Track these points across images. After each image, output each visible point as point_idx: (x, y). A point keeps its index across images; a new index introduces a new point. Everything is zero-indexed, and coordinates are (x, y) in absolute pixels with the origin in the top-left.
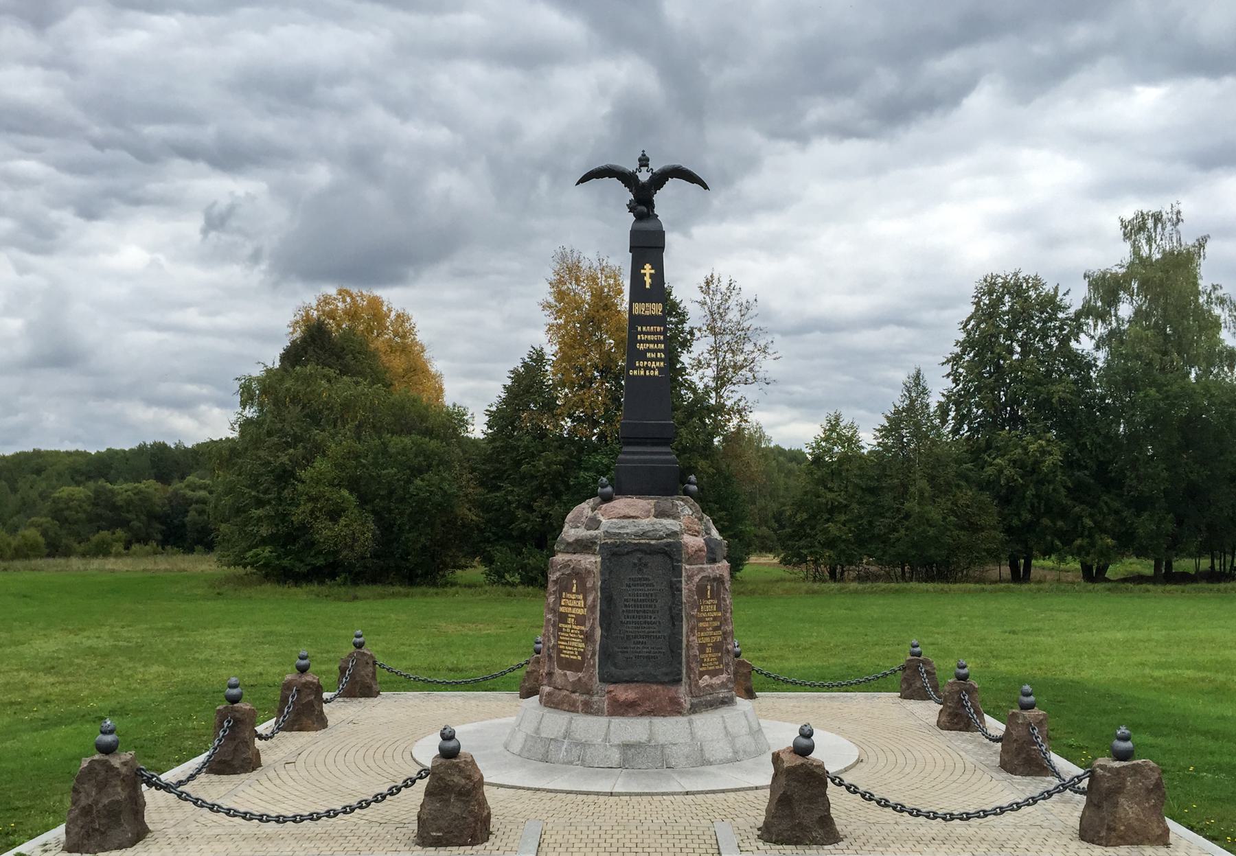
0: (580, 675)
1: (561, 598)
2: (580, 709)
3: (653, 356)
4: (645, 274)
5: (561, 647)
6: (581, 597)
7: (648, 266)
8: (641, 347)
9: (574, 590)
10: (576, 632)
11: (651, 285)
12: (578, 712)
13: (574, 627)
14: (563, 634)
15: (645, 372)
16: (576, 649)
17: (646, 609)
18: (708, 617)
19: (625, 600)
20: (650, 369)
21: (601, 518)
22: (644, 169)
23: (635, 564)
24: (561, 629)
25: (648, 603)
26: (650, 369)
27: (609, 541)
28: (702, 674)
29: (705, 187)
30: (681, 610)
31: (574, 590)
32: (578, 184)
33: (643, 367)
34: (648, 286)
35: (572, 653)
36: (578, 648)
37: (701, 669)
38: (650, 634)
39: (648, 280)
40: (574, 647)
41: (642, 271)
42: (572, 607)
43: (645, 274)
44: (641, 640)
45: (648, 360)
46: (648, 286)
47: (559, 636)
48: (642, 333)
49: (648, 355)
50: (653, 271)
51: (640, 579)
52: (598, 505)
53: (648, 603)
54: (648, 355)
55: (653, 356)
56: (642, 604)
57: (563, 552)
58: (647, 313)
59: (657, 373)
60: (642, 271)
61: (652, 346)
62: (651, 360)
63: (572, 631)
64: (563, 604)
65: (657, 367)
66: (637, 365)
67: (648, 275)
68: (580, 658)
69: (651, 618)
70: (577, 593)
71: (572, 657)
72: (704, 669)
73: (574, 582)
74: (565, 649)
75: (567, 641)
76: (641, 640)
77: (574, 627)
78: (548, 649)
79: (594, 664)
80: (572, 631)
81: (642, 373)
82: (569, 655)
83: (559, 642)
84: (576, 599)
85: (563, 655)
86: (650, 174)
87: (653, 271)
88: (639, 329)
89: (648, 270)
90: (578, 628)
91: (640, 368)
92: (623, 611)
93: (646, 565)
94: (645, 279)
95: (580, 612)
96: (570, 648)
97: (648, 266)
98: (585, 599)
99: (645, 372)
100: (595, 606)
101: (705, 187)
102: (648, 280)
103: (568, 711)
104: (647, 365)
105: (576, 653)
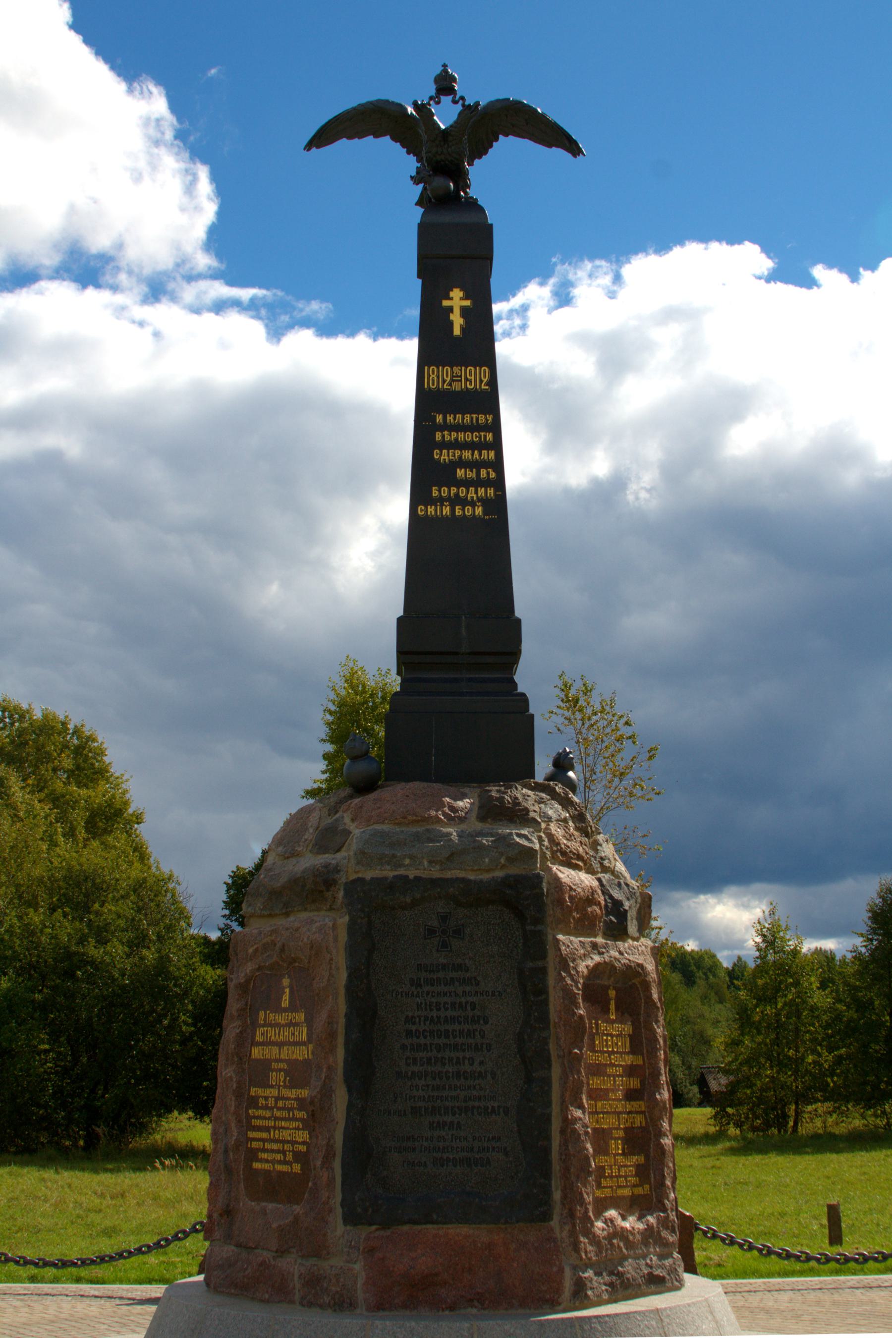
0: (297, 1209)
1: (255, 1025)
2: (297, 1297)
3: (471, 474)
4: (450, 309)
5: (255, 1145)
6: (301, 1017)
7: (456, 294)
8: (444, 456)
9: (285, 1003)
10: (288, 1104)
11: (462, 329)
12: (292, 1302)
13: (286, 1093)
14: (259, 1112)
15: (453, 511)
16: (287, 1147)
17: (460, 1040)
18: (612, 1065)
19: (408, 1020)
20: (464, 502)
21: (352, 827)
22: (446, 100)
23: (431, 932)
24: (253, 1102)
25: (466, 1027)
26: (464, 502)
27: (369, 875)
28: (601, 1206)
29: (573, 148)
30: (545, 1041)
31: (285, 1003)
32: (309, 146)
33: (449, 499)
34: (457, 331)
35: (279, 1157)
36: (293, 1143)
37: (598, 1193)
38: (470, 1104)
39: (457, 321)
40: (284, 1142)
41: (446, 303)
42: (280, 1045)
43: (450, 309)
44: (448, 1119)
45: (459, 483)
46: (457, 331)
47: (249, 1118)
48: (445, 427)
49: (460, 473)
50: (467, 303)
51: (444, 967)
52: (341, 802)
53: (466, 1027)
54: (460, 473)
55: (471, 474)
56: (450, 1027)
57: (262, 916)
58: (457, 387)
59: (479, 511)
60: (446, 303)
61: (467, 455)
62: (467, 483)
63: (280, 1104)
64: (258, 1038)
65: (479, 500)
66: (435, 493)
67: (457, 311)
68: (297, 1168)
69: (472, 1061)
70: (293, 1008)
71: (280, 1168)
72: (607, 1192)
73: (286, 982)
74: (264, 1150)
75: (267, 1129)
76: (448, 1119)
77: (286, 1093)
78: (226, 1151)
79: (331, 1181)
80: (280, 1104)
81: (446, 511)
82: (273, 1162)
83: (251, 1134)
84: (291, 1024)
85: (256, 1165)
86: (459, 107)
87: (467, 303)
88: (439, 418)
89: (457, 299)
90: (292, 1093)
91: (441, 500)
92: (404, 1047)
93: (458, 932)
94: (452, 317)
95: (301, 1054)
96: (275, 1146)
97: (456, 294)
98: (309, 1021)
99: (453, 511)
100: (332, 1035)
101: (573, 148)
102: (457, 321)
103: (279, 1302)
104: (457, 495)
105: (289, 1157)
